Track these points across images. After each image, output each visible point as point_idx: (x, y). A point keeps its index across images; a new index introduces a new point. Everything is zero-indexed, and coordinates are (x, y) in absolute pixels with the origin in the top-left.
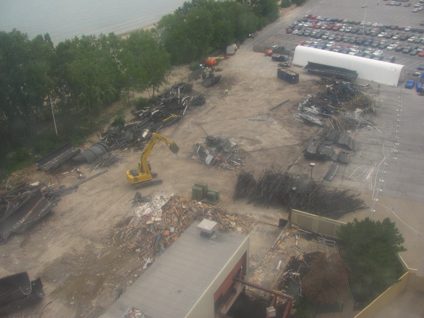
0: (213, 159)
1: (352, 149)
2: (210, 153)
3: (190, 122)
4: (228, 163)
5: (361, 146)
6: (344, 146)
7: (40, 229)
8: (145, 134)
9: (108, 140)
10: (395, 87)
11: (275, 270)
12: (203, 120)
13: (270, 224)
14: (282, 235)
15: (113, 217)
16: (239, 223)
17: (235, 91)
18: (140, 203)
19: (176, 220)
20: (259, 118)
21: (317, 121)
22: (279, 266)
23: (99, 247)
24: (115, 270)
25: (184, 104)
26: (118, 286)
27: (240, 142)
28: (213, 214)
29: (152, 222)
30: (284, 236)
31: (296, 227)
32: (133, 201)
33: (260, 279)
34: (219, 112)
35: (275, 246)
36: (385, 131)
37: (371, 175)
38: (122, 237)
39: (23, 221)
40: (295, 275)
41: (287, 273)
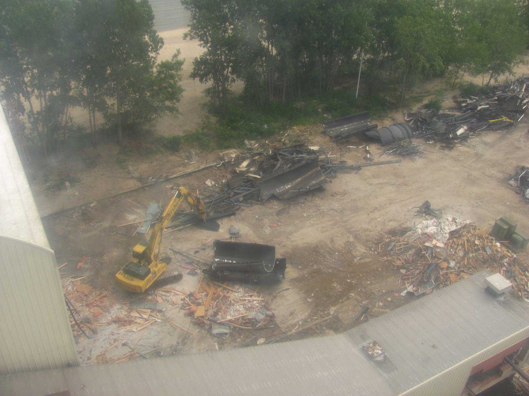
7: (304, 203)
8: (460, 132)
9: (413, 124)
15: (388, 220)
18: (426, 215)
19: (461, 254)
23: (361, 249)
24: (368, 283)
25: (524, 108)
28: (509, 264)
29: (432, 246)
32: (418, 209)
38: (390, 248)
39: (289, 186)
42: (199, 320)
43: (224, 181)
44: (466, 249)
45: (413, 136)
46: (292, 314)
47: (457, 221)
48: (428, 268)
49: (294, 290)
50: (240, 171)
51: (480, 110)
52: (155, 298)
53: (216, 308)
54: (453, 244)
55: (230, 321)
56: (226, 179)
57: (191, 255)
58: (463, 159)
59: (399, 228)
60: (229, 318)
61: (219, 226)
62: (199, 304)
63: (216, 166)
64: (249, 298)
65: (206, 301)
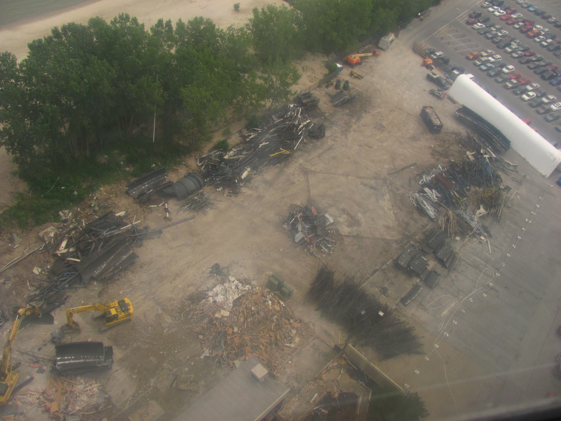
0: (303, 238)
1: (447, 267)
2: (302, 230)
3: (297, 165)
4: (316, 247)
5: (459, 265)
6: (441, 262)
7: (119, 279)
8: (244, 175)
9: (204, 169)
10: (546, 178)
11: (308, 402)
12: (312, 165)
13: (326, 344)
14: (330, 365)
15: (187, 285)
16: (299, 333)
17: (364, 124)
18: (217, 275)
19: (242, 319)
20: (372, 182)
21: (431, 212)
22: (313, 399)
23: (168, 319)
24: (176, 352)
25: (299, 134)
26: (175, 370)
27: (339, 217)
28: (278, 320)
29: (220, 317)
30: (331, 366)
31: (347, 358)
32: (210, 269)
33: (293, 408)
34: (334, 158)
35: (319, 376)
36: (496, 249)
37: (449, 310)
38: (190, 317)
39: (105, 265)
40: (323, 412)
41: (317, 407)
42: (55, 415)
43: (49, 267)
44: (246, 315)
45: (205, 184)
46: (123, 392)
47: (239, 287)
48: (219, 335)
49: (122, 370)
50: (61, 254)
51: (262, 147)
52: (15, 402)
53: (67, 403)
54: (236, 312)
55: (79, 410)
56: (50, 264)
57: (36, 353)
58: (247, 204)
59: (196, 292)
60: (78, 408)
61: (53, 317)
62: (52, 401)
63: (38, 250)
64: (90, 388)
65: (57, 396)
